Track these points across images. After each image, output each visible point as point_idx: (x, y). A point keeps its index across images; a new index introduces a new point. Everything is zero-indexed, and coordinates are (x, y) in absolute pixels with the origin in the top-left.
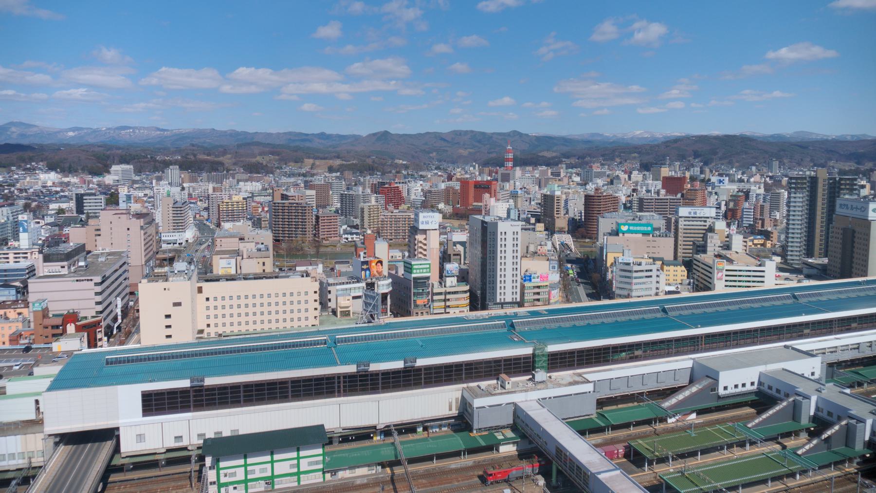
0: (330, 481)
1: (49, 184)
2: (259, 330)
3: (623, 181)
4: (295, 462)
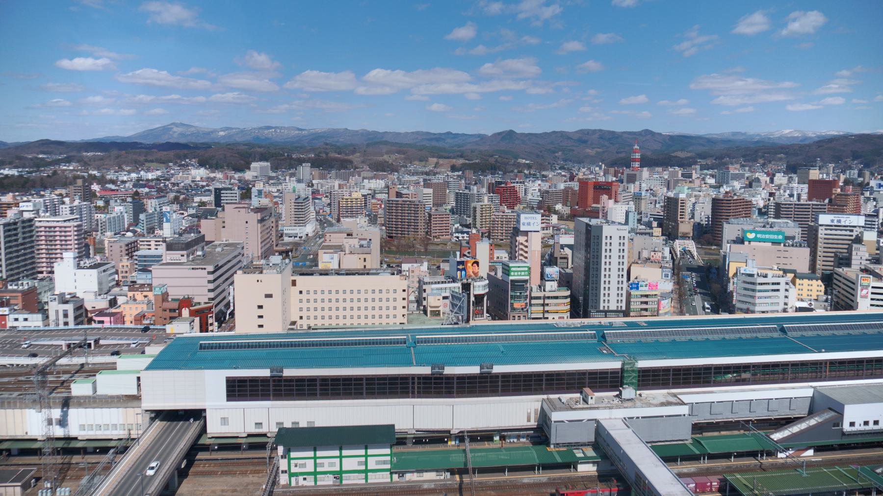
0: (397, 482)
1: (198, 178)
2: (348, 325)
3: (763, 184)
4: (363, 459)
